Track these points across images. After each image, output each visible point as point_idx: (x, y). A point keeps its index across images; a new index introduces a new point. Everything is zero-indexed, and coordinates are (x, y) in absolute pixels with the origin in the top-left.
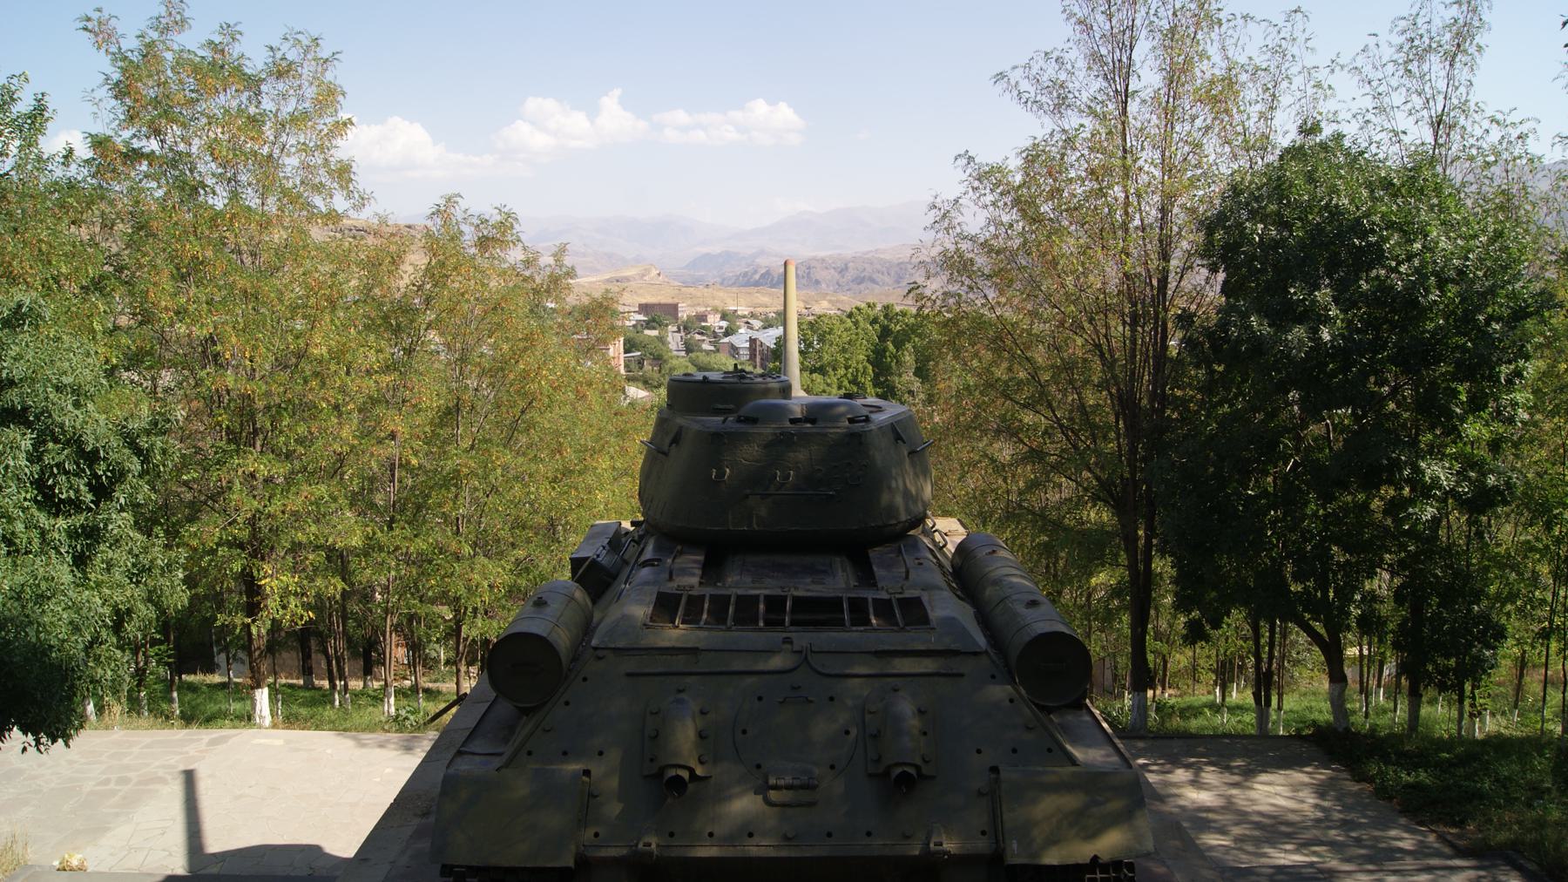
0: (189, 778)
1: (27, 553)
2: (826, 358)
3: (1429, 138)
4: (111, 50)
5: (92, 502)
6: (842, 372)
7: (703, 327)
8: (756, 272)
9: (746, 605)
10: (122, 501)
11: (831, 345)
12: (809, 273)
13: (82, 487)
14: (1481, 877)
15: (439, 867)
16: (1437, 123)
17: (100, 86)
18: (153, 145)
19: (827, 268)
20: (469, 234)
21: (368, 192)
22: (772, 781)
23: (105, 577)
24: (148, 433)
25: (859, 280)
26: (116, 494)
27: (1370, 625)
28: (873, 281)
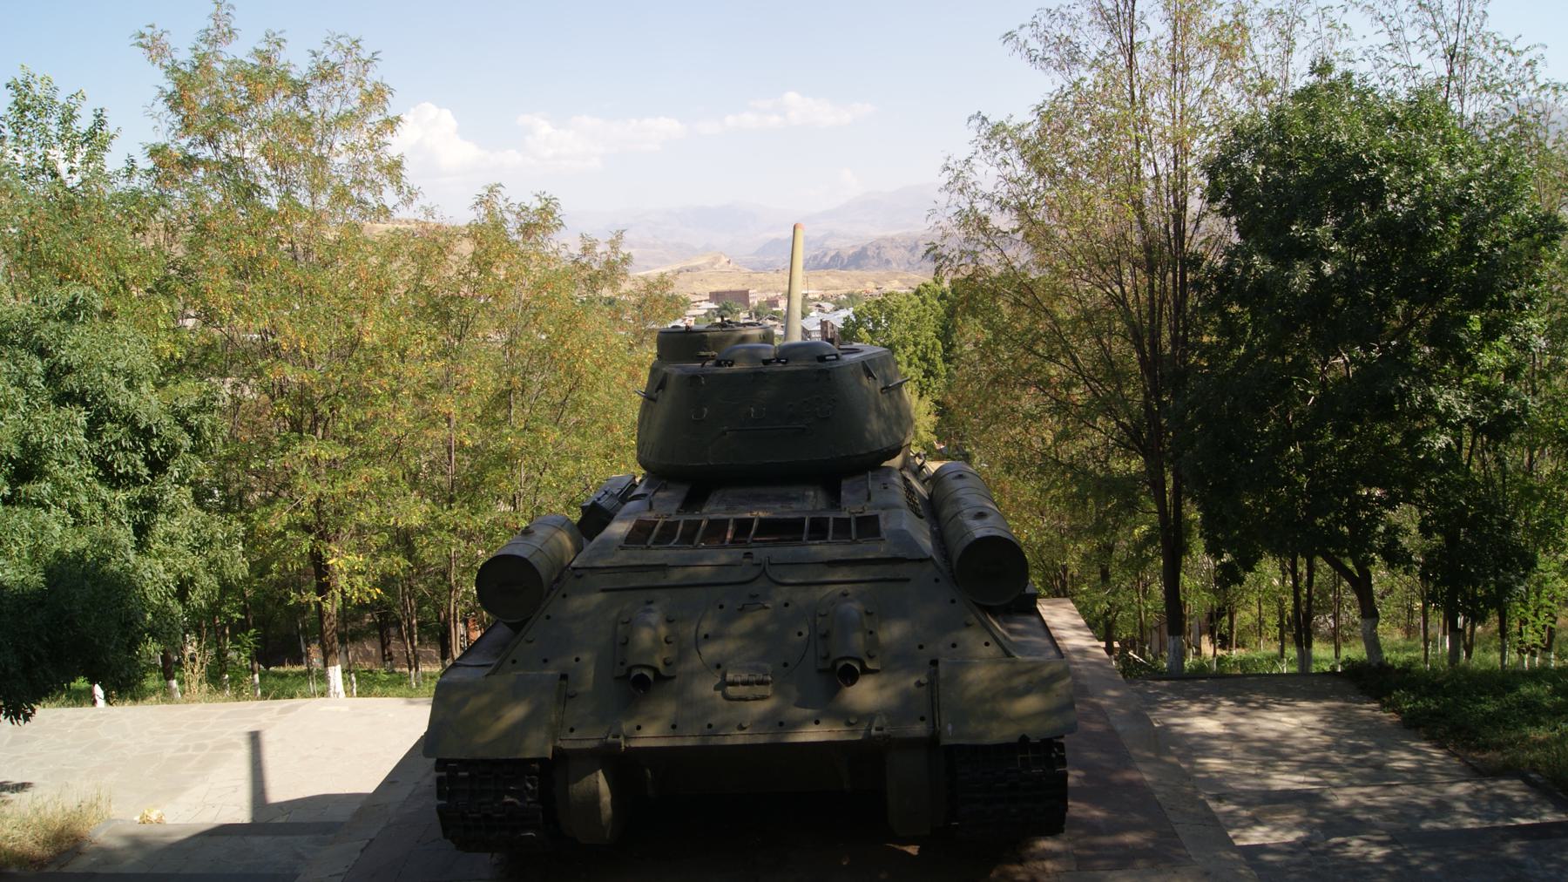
0: (255, 739)
1: (91, 523)
2: (895, 336)
3: (1443, 70)
4: (164, 64)
5: (148, 475)
6: (911, 349)
7: (775, 313)
8: (825, 255)
9: (717, 528)
10: (176, 474)
11: (899, 323)
12: (879, 254)
13: (139, 462)
14: (1478, 791)
15: (433, 761)
16: (1451, 55)
17: (157, 99)
18: (207, 152)
19: (896, 247)
20: (512, 226)
21: (416, 187)
22: (730, 677)
23: (168, 547)
24: (197, 410)
26: (170, 468)
27: (1395, 557)
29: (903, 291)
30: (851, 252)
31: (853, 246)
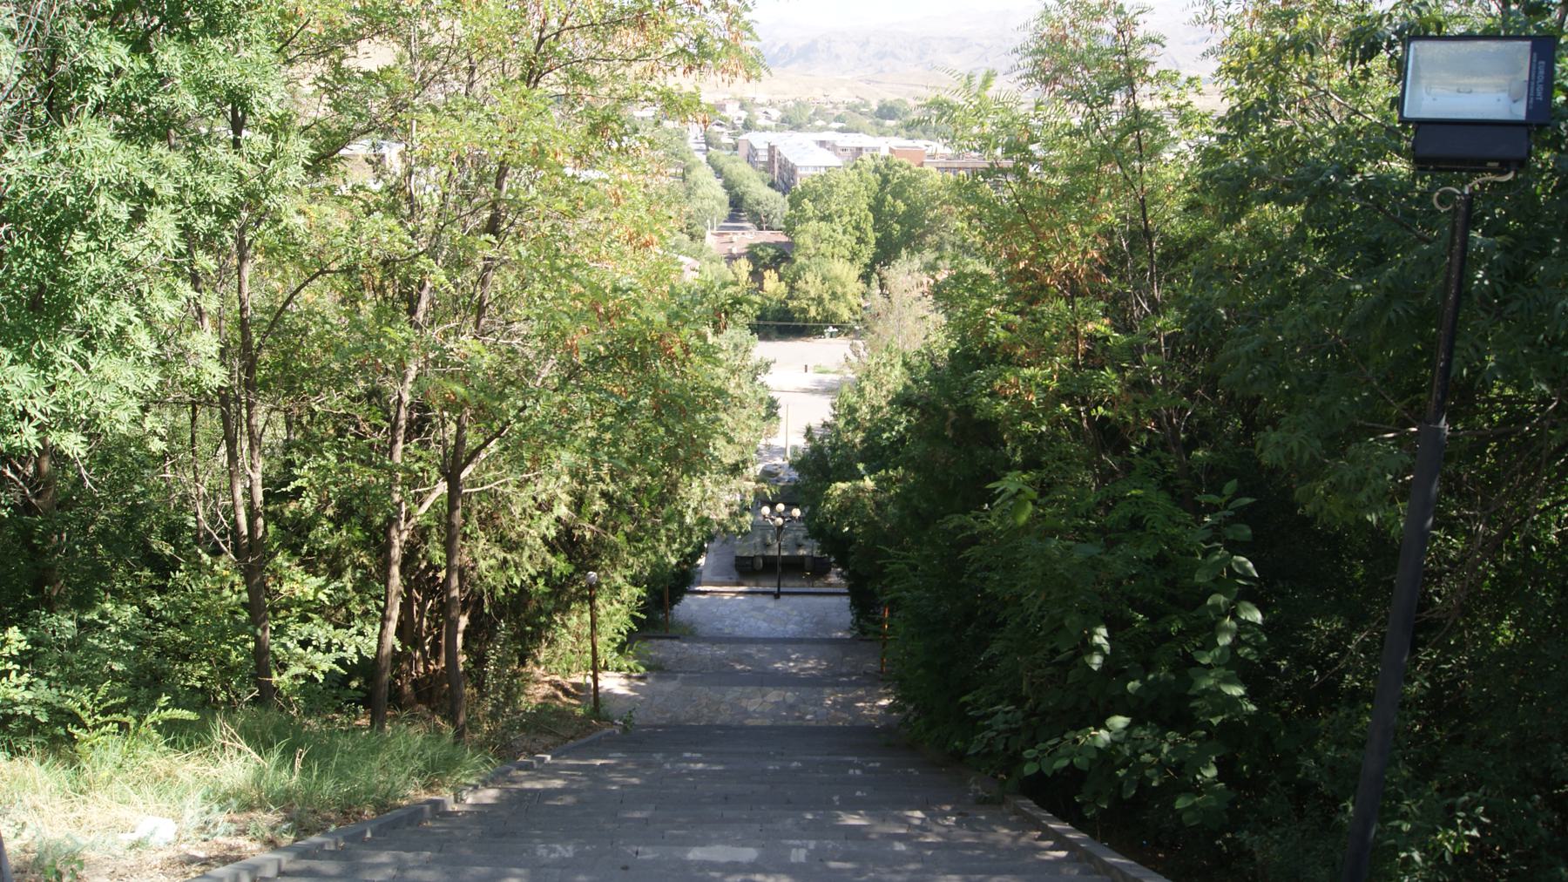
6: (846, 219)
8: (774, 44)
25: (881, 56)
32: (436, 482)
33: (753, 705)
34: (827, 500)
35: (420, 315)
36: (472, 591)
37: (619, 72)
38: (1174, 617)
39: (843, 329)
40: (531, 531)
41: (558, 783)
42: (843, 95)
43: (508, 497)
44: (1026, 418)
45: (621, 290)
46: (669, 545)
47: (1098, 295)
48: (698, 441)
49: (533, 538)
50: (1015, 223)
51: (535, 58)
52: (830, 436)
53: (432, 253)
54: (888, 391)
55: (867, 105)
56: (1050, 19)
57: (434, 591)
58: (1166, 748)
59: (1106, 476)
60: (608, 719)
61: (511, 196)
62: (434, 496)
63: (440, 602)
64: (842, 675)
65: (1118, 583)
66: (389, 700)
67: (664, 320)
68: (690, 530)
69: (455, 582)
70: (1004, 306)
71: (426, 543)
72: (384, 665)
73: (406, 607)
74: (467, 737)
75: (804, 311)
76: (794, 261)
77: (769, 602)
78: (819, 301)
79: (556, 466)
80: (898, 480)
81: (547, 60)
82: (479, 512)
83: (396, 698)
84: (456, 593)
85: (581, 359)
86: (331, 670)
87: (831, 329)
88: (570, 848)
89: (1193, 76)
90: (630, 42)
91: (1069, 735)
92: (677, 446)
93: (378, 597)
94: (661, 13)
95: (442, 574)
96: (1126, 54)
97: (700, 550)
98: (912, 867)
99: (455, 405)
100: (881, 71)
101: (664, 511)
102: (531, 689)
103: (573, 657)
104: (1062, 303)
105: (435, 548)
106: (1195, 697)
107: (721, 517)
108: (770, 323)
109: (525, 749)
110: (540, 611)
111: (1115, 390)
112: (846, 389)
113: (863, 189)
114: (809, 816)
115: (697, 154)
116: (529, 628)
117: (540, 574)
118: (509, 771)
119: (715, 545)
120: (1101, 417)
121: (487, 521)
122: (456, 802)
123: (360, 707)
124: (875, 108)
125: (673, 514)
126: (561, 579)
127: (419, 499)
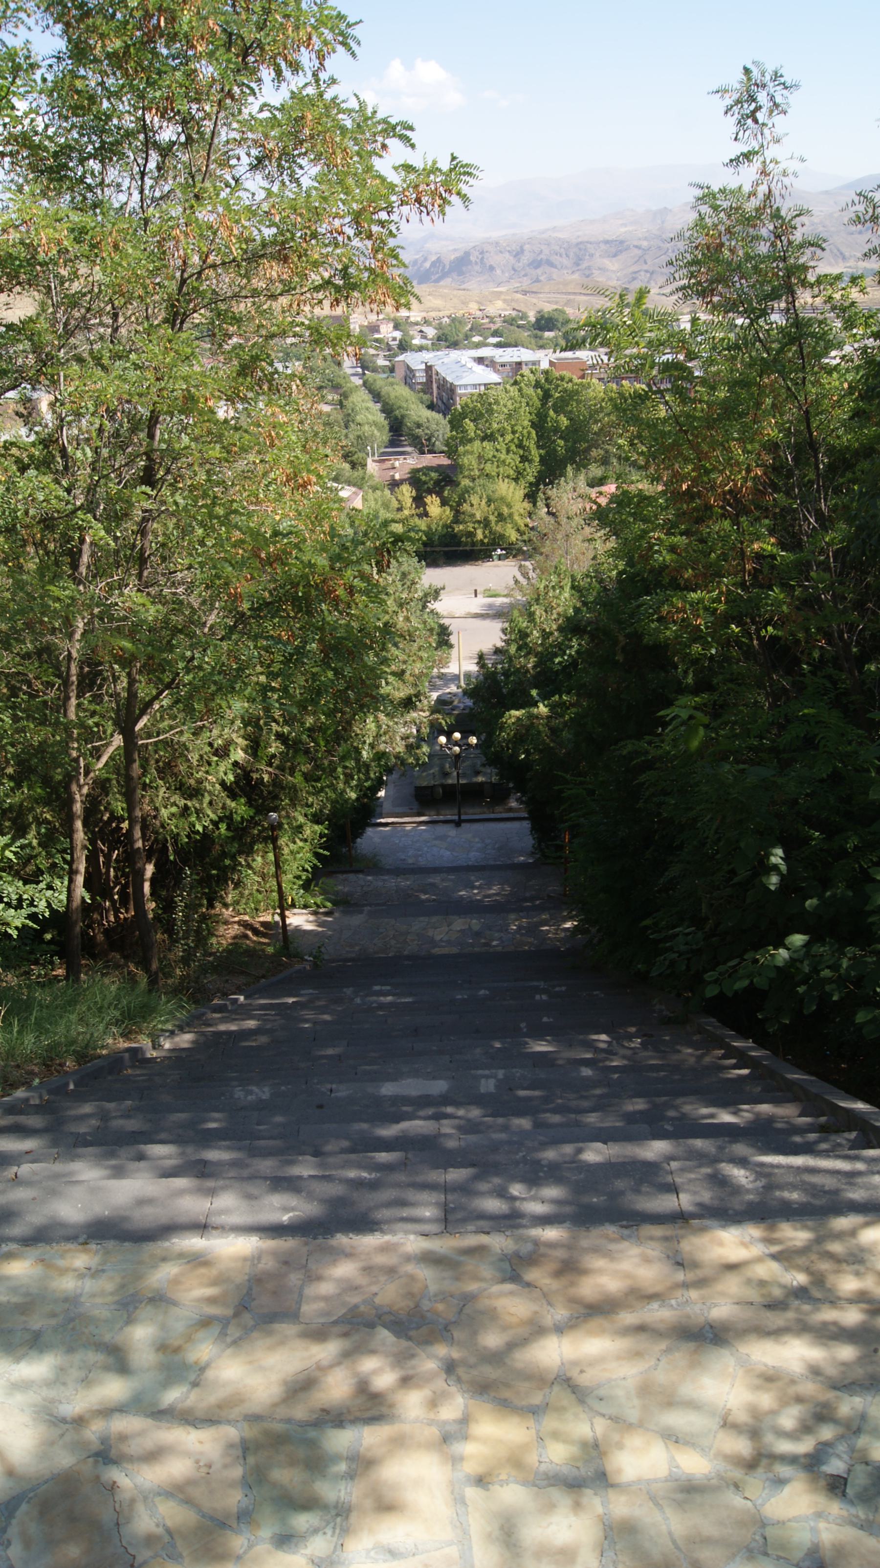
6: (509, 437)
7: (377, 340)
8: (425, 260)
12: (482, 259)
25: (536, 264)
28: (551, 264)
29: (507, 313)
30: (453, 257)
31: (455, 250)
32: (112, 736)
33: (439, 934)
34: (502, 729)
35: (83, 570)
36: (156, 840)
37: (265, 307)
38: (850, 833)
39: (512, 551)
40: (210, 778)
41: (252, 1024)
42: (498, 308)
43: (184, 745)
44: (695, 641)
45: (281, 534)
46: (346, 782)
47: (766, 511)
48: (368, 682)
49: (212, 784)
50: (676, 444)
51: (178, 300)
52: (502, 662)
53: (90, 507)
54: (559, 614)
55: (524, 317)
56: (704, 227)
57: (119, 841)
58: (845, 963)
59: (777, 695)
60: (299, 956)
61: (164, 446)
62: (111, 749)
63: (125, 852)
64: (526, 900)
65: (795, 802)
66: (83, 950)
67: (326, 563)
68: (367, 766)
69: (138, 833)
70: (670, 528)
71: (107, 795)
72: (74, 917)
73: (91, 860)
74: (161, 983)
75: (471, 535)
76: (458, 484)
77: (451, 831)
78: (486, 523)
79: (229, 714)
80: (572, 705)
81: (191, 301)
82: (157, 761)
83: (89, 948)
84: (139, 844)
85: (245, 606)
86: (24, 926)
87: (499, 552)
88: (266, 1089)
89: (856, 275)
90: (274, 274)
91: (748, 956)
92: (347, 688)
93: (64, 851)
94: (304, 245)
95: (125, 825)
96: (784, 259)
97: (379, 784)
98: (598, 1092)
99: (126, 661)
100: (538, 281)
101: (340, 749)
102: (221, 930)
103: (260, 897)
104: (727, 524)
105: (116, 800)
106: (873, 913)
107: (398, 749)
108: (438, 549)
109: (218, 990)
110: (224, 855)
111: (785, 608)
112: (516, 613)
113: (524, 405)
114: (498, 1045)
115: (353, 379)
116: (214, 872)
117: (221, 819)
118: (203, 1014)
119: (395, 776)
120: (771, 636)
121: (166, 770)
122: (154, 1048)
123: (56, 958)
124: (533, 319)
125: (349, 752)
126: (242, 823)
127: (97, 753)
